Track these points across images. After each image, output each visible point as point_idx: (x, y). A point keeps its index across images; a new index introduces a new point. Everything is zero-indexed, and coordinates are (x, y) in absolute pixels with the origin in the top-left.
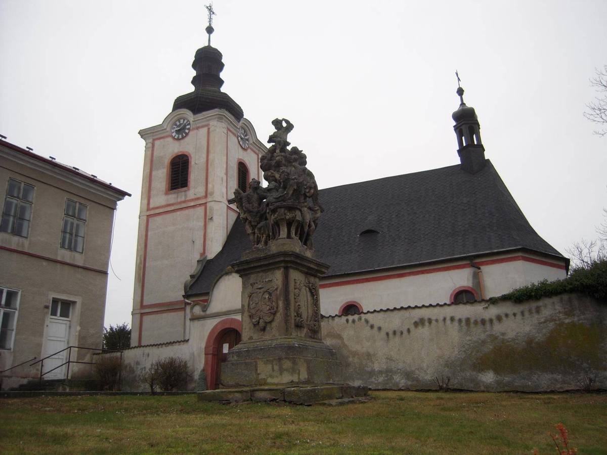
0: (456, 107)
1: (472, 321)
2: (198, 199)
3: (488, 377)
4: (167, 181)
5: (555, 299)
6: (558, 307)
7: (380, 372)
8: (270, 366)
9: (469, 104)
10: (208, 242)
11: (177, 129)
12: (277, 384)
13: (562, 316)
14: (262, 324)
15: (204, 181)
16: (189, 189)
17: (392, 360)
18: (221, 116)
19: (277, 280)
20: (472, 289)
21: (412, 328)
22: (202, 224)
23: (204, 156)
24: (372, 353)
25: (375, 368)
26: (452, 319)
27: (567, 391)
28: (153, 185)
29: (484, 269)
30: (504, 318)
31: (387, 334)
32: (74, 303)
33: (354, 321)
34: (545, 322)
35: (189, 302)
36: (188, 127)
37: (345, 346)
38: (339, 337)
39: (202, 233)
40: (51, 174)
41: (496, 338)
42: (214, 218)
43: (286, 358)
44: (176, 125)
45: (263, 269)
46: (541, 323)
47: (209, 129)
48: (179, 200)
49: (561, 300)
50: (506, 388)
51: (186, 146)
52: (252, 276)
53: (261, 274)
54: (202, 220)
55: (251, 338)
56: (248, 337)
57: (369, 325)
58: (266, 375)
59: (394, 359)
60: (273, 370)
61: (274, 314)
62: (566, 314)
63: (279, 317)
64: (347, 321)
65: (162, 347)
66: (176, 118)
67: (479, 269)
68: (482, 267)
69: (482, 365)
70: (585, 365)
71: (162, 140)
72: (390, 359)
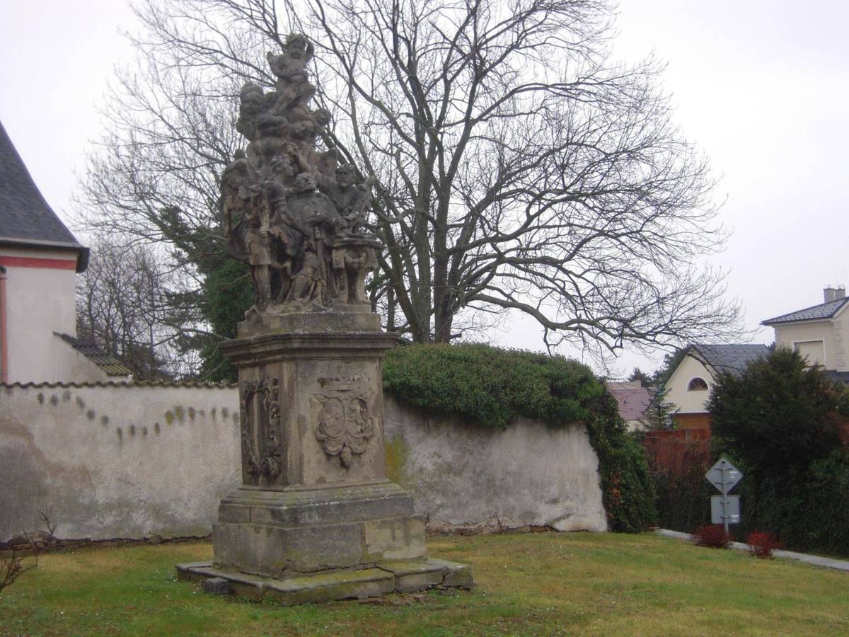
7: (109, 507)
17: (129, 483)
19: (369, 380)
21: (163, 422)
24: (92, 468)
25: (97, 498)
31: (120, 431)
33: (54, 401)
37: (37, 452)
38: (24, 432)
45: (346, 355)
52: (320, 363)
53: (336, 363)
55: (321, 480)
56: (317, 478)
57: (86, 411)
58: (381, 547)
59: (132, 481)
60: (394, 538)
64: (41, 398)
72: (124, 481)
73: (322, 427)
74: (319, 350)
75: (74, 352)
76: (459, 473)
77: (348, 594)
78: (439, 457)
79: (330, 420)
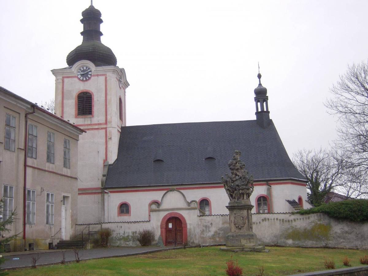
0: (256, 86)
1: (285, 220)
2: (100, 124)
3: (290, 242)
4: (76, 108)
5: (315, 214)
6: (316, 218)
8: (246, 241)
9: (264, 85)
10: (108, 153)
11: (82, 73)
12: (249, 246)
13: (317, 221)
14: (240, 227)
15: (104, 113)
16: (93, 117)
18: (114, 70)
20: (267, 196)
21: (261, 222)
22: (104, 141)
23: (104, 95)
26: (277, 219)
27: (317, 247)
28: (65, 110)
29: (273, 186)
30: (296, 220)
32: (68, 197)
34: (311, 223)
35: (108, 192)
36: (90, 73)
39: (104, 147)
40: (54, 123)
41: (293, 227)
42: (113, 138)
43: (252, 238)
44: (80, 70)
46: (309, 223)
47: (106, 78)
48: (86, 123)
49: (317, 215)
50: (296, 246)
51: (91, 86)
53: (238, 211)
54: (104, 138)
60: (247, 242)
61: (244, 224)
62: (318, 220)
63: (246, 225)
65: (131, 223)
66: (80, 65)
67: (271, 186)
68: (272, 186)
69: (288, 237)
70: (323, 239)
71: (70, 79)
73: (234, 221)
74: (234, 208)
75: (289, 204)
76: (350, 233)
77: (233, 250)
78: (343, 229)
79: (236, 221)
